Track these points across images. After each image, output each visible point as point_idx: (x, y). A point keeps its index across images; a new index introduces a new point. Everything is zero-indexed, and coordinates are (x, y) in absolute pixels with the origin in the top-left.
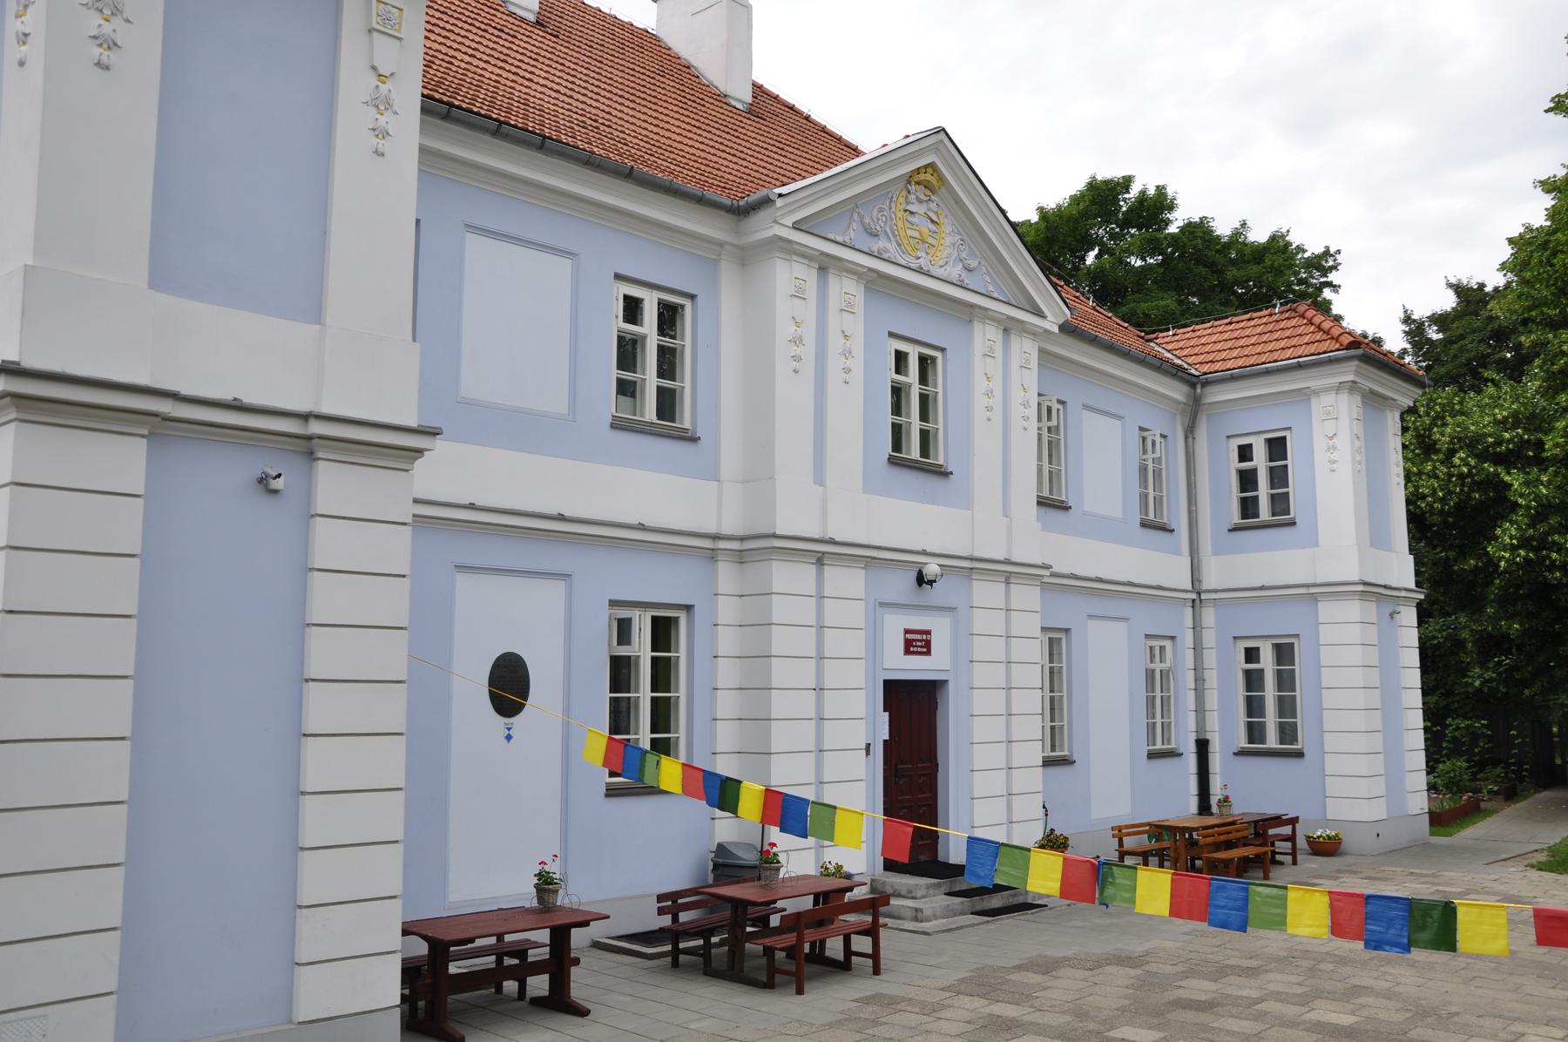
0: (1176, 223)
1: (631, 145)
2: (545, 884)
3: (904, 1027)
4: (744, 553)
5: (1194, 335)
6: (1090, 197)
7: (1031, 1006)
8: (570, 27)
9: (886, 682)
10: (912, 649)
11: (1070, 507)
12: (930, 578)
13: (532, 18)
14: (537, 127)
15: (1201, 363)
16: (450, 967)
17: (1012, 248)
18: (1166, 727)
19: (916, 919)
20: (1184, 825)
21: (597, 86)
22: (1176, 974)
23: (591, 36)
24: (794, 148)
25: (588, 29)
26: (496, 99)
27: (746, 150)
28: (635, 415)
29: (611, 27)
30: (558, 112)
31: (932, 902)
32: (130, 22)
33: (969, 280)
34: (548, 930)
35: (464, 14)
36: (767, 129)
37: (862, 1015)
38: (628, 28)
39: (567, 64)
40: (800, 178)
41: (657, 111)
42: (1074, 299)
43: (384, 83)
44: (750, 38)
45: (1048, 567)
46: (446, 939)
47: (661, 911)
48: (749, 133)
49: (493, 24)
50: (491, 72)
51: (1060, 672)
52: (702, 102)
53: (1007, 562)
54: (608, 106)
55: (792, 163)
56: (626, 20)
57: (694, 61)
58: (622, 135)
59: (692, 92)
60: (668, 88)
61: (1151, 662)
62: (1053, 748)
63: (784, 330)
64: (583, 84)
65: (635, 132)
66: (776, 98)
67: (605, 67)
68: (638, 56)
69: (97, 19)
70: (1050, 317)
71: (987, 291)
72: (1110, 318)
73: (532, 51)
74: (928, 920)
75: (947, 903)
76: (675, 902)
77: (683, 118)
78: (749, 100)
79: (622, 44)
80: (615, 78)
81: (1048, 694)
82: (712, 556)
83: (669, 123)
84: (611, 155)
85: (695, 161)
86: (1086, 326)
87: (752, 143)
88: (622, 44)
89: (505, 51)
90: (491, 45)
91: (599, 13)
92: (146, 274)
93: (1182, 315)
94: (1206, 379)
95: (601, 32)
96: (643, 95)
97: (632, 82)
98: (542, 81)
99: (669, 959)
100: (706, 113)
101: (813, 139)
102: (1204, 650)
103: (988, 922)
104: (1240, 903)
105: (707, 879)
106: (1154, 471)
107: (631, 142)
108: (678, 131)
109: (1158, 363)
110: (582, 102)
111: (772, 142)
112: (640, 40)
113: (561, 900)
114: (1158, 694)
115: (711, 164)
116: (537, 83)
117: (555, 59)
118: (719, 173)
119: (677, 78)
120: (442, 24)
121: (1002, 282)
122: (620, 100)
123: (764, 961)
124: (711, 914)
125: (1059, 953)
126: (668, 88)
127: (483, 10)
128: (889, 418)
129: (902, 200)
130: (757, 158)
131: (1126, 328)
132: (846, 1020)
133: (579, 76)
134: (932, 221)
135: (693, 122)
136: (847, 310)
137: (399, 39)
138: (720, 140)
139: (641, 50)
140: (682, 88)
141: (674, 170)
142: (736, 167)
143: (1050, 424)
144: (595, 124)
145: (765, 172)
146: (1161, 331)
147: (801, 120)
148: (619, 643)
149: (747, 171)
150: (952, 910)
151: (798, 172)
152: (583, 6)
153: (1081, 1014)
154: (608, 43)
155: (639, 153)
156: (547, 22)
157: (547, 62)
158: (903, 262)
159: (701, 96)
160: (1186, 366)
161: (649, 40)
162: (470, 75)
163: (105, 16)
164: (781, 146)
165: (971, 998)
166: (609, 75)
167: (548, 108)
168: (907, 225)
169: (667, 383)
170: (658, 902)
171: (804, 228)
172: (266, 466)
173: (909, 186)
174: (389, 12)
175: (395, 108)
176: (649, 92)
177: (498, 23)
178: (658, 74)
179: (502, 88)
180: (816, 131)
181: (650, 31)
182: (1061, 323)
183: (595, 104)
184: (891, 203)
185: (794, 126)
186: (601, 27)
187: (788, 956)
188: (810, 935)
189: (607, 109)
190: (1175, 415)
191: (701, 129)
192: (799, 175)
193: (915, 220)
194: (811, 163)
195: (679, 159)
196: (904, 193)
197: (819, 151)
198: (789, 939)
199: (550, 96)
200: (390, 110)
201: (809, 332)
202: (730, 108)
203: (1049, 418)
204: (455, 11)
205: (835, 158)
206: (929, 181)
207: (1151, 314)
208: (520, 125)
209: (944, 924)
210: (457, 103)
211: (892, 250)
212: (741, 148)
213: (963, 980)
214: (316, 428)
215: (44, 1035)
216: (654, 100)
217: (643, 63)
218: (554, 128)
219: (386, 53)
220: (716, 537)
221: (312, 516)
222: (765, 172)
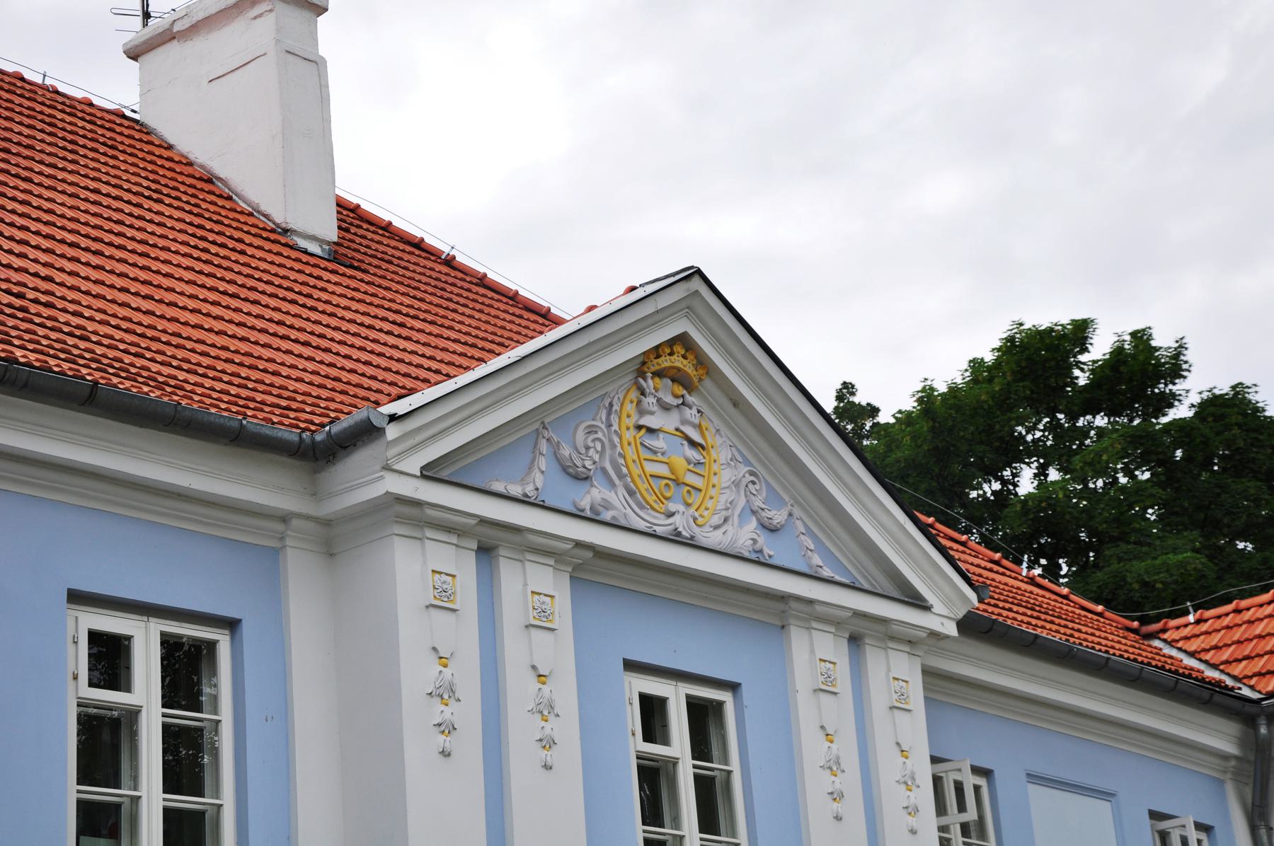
1: (94, 338)
5: (1238, 619)
6: (1014, 366)
21: (47, 237)
24: (424, 320)
33: (772, 549)
38: (84, 109)
40: (440, 378)
41: (149, 269)
42: (989, 565)
48: (335, 300)
52: (239, 246)
55: (421, 349)
56: (79, 95)
57: (219, 168)
58: (75, 321)
59: (217, 228)
60: (169, 223)
65: (105, 312)
66: (387, 227)
67: (37, 190)
68: (106, 164)
70: (938, 607)
71: (810, 567)
72: (1100, 615)
77: (202, 279)
78: (332, 234)
79: (72, 142)
80: (60, 210)
83: (173, 290)
84: (52, 362)
85: (227, 361)
86: (1017, 620)
87: (342, 318)
88: (72, 142)
91: (19, 84)
93: (1220, 578)
95: (27, 121)
96: (118, 241)
100: (249, 266)
101: (462, 301)
108: (192, 304)
111: (381, 313)
112: (109, 134)
119: (188, 203)
121: (835, 544)
122: (71, 252)
126: (169, 223)
129: (630, 408)
131: (1100, 615)
134: (693, 444)
135: (222, 286)
136: (540, 624)
139: (111, 152)
140: (197, 221)
141: (186, 381)
142: (310, 366)
143: (965, 817)
145: (370, 371)
149: (334, 372)
151: (434, 365)
154: (42, 141)
155: (111, 354)
158: (641, 525)
159: (237, 234)
160: (1230, 682)
161: (126, 132)
164: (399, 319)
166: (47, 205)
167: (67, 324)
168: (645, 454)
171: (444, 474)
173: (641, 381)
178: (149, 198)
180: (466, 285)
182: (960, 615)
184: (609, 414)
185: (424, 279)
186: (26, 112)
190: (1222, 782)
191: (239, 297)
192: (437, 372)
193: (658, 443)
194: (459, 348)
196: (634, 394)
197: (474, 323)
202: (294, 254)
203: (962, 808)
205: (507, 334)
206: (679, 369)
207: (1156, 581)
211: (617, 502)
212: (319, 329)
217: (115, 177)
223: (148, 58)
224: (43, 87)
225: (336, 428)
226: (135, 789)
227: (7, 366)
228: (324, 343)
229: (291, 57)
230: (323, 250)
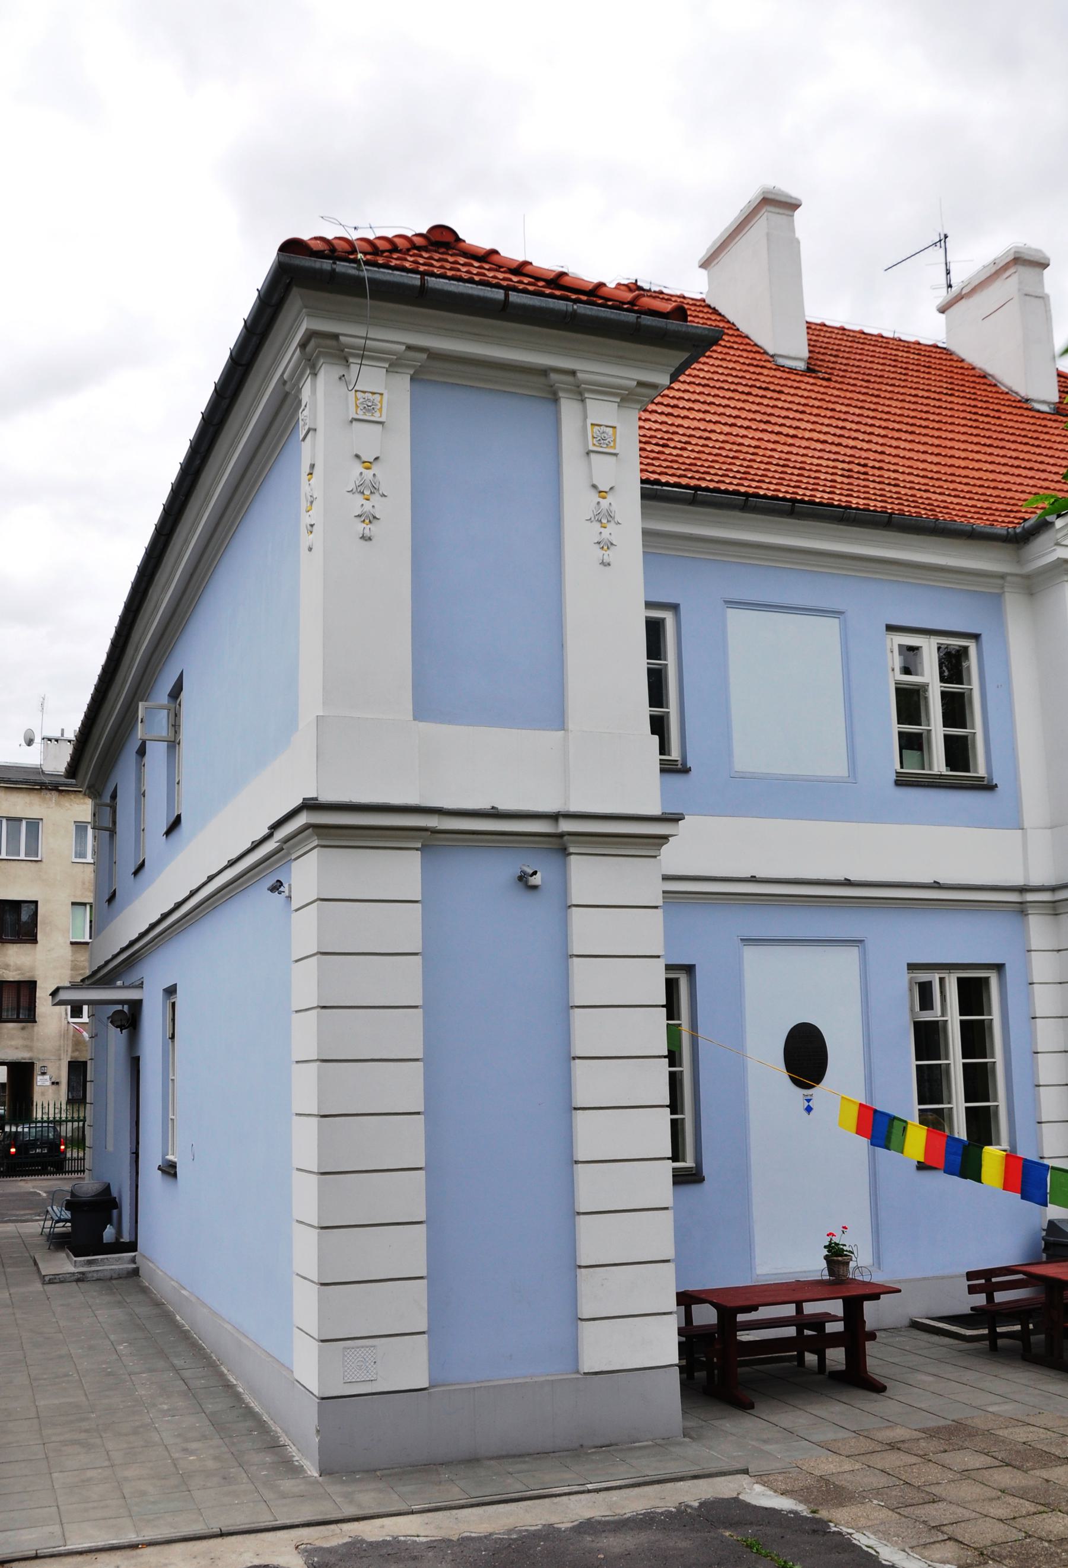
2: (836, 1256)
13: (801, 366)
28: (924, 769)
32: (385, 496)
38: (916, 348)
39: (838, 407)
43: (604, 498)
46: (732, 1305)
47: (972, 1290)
57: (990, 369)
69: (359, 499)
76: (988, 1280)
78: (1055, 397)
82: (1022, 910)
91: (880, 340)
92: (410, 707)
98: (807, 435)
115: (1000, 486)
137: (615, 455)
152: (863, 336)
163: (366, 496)
172: (524, 865)
174: (603, 432)
181: (940, 345)
200: (612, 522)
202: (1031, 414)
214: (565, 826)
215: (375, 1362)
219: (604, 470)
220: (1022, 890)
221: (570, 907)
223: (951, 311)
224: (894, 339)
225: (1027, 524)
226: (929, 726)
227: (844, 512)
228: (1042, 467)
229: (1028, 298)
230: (1050, 408)
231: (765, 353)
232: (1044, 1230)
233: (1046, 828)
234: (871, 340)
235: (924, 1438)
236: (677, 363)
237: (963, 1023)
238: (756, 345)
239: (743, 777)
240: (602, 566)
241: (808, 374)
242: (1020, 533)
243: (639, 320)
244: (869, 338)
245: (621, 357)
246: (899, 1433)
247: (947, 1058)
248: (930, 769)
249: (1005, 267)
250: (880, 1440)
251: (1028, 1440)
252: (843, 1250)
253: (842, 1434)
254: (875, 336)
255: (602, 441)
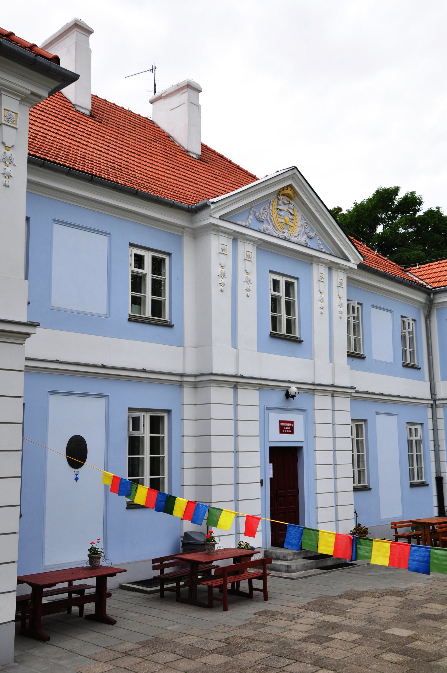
0: (423, 209)
3: (278, 627)
4: (197, 383)
5: (429, 268)
7: (345, 617)
8: (108, 117)
9: (271, 448)
10: (284, 431)
11: (365, 357)
12: (292, 394)
13: (88, 113)
14: (90, 170)
15: (433, 282)
16: (43, 600)
17: (333, 227)
18: (419, 471)
19: (288, 571)
20: (429, 522)
22: (423, 601)
23: (119, 122)
24: (222, 177)
25: (117, 118)
26: (69, 155)
27: (197, 179)
28: (141, 314)
29: (129, 117)
30: (100, 162)
31: (296, 562)
33: (310, 243)
34: (95, 578)
35: (53, 112)
36: (209, 168)
37: (257, 622)
38: (138, 117)
39: (106, 137)
40: (225, 193)
42: (367, 251)
43: (8, 150)
44: (199, 122)
45: (354, 388)
47: (154, 568)
48: (199, 170)
49: (68, 117)
50: (66, 142)
51: (362, 442)
52: (175, 155)
53: (332, 386)
54: (127, 158)
55: (221, 185)
57: (172, 134)
58: (133, 173)
61: (411, 436)
62: (360, 482)
63: (216, 270)
64: (114, 147)
66: (214, 152)
67: (125, 138)
70: (352, 261)
71: (320, 248)
72: (386, 260)
73: (88, 131)
74: (294, 572)
75: (304, 563)
76: (161, 563)
77: (165, 163)
78: (200, 153)
81: (356, 454)
82: (181, 385)
83: (158, 166)
84: (127, 184)
86: (373, 265)
89: (74, 130)
90: (67, 128)
91: (123, 110)
94: (436, 290)
95: (124, 120)
97: (139, 145)
98: (93, 146)
99: (159, 594)
100: (178, 160)
101: (233, 172)
102: (438, 430)
103: (325, 573)
104: (426, 559)
105: (180, 551)
106: (409, 338)
107: (138, 176)
108: (162, 170)
109: (410, 283)
110: (113, 156)
111: (211, 175)
112: (144, 124)
113: (102, 562)
114: (415, 453)
115: (180, 187)
116: (90, 147)
117: (100, 134)
118: (184, 191)
119: (163, 143)
120: (41, 117)
122: (133, 155)
123: (207, 594)
124: (182, 569)
125: (362, 589)
126: (158, 148)
127: (63, 110)
128: (270, 314)
129: (275, 203)
130: (203, 183)
131: (394, 265)
132: (248, 624)
133: (112, 143)
134: (291, 214)
136: (248, 259)
137: (16, 128)
138: (184, 174)
139: (144, 128)
140: (165, 148)
142: (192, 188)
143: (354, 315)
144: (119, 168)
145: (207, 190)
146: (413, 266)
147: (227, 163)
148: (133, 430)
149: (198, 190)
150: (307, 567)
151: (224, 189)
152: (115, 106)
153: (371, 621)
155: (142, 182)
156: (96, 115)
157: (95, 136)
158: (276, 235)
159: (175, 152)
160: (425, 284)
161: (148, 123)
162: (56, 143)
164: (216, 176)
165: (314, 612)
166: (128, 142)
167: (96, 160)
168: (278, 216)
169: (157, 298)
170: (153, 563)
171: (225, 218)
173: (279, 196)
174: (10, 115)
175: (15, 163)
176: (148, 150)
177: (70, 116)
178: (153, 141)
179: (72, 150)
180: (234, 168)
181: (149, 118)
182: (358, 264)
183: (120, 157)
184: (270, 205)
187: (221, 591)
188: (231, 579)
189: (126, 160)
190: (420, 309)
192: (225, 191)
193: (282, 213)
194: (231, 185)
195: (163, 184)
196: (276, 200)
198: (220, 581)
199: (97, 154)
200: (12, 164)
201: (228, 271)
202: (189, 158)
203: (354, 312)
204: (48, 110)
206: (289, 194)
207: (411, 258)
208: (80, 169)
209: (302, 574)
210: (48, 158)
212: (195, 178)
213: (310, 603)
216: (150, 154)
218: (98, 170)
220: (182, 375)
222: (207, 190)
225: (198, 205)
229: (191, 104)
230: (197, 157)
231: (70, 103)
232: (182, 537)
233: (194, 347)
234: (118, 109)
235: (140, 648)
236: (53, 87)
237: (151, 438)
238: (65, 98)
239: (56, 309)
240: (4, 187)
241: (91, 118)
242: (194, 208)
243: (36, 58)
244: (118, 108)
245: (23, 76)
246: (128, 646)
247: (143, 454)
248: (144, 314)
249: (183, 88)
250: (119, 650)
251: (191, 643)
252: (98, 551)
253: (100, 650)
254: (120, 107)
255: (9, 120)
